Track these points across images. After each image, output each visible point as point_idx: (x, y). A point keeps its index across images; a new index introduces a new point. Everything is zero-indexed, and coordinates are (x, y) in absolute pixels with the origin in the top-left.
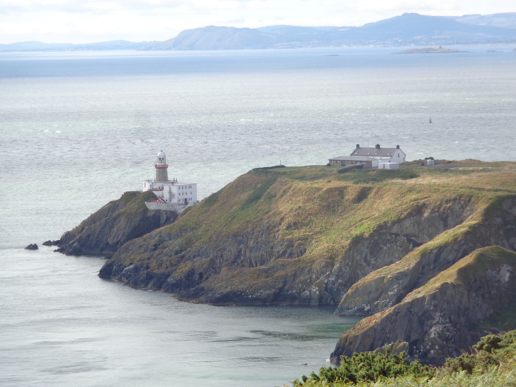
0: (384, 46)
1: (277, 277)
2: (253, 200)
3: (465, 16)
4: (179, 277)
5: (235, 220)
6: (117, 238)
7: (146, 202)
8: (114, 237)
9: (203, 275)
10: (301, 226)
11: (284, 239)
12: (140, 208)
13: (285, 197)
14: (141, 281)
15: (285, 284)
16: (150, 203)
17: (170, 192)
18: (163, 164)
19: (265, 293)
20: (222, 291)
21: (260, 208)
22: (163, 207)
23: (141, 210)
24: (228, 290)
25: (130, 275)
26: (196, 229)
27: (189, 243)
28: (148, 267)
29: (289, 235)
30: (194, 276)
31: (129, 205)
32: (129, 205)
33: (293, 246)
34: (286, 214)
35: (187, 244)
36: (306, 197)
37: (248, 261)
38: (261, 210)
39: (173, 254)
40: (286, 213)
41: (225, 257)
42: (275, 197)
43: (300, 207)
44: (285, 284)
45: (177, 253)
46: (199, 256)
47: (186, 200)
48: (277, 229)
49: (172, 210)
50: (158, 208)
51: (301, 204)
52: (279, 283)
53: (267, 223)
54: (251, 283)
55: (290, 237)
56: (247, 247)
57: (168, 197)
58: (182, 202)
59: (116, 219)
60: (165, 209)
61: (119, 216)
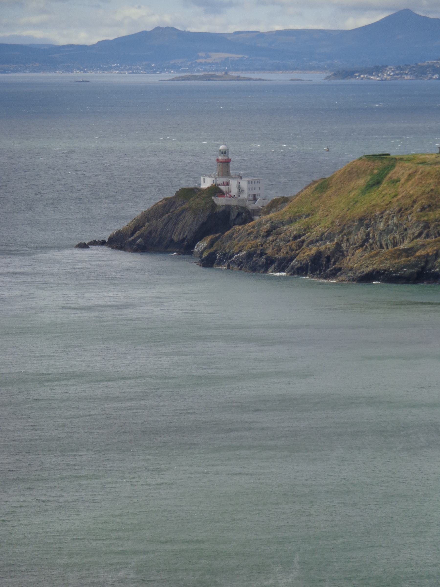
0: (133, 73)
1: (419, 257)
2: (374, 185)
3: (236, 33)
4: (305, 261)
5: (358, 204)
6: (184, 234)
7: (213, 198)
8: (180, 234)
9: (331, 258)
10: (436, 208)
11: (419, 221)
12: (208, 203)
13: (413, 180)
14: (260, 266)
15: (427, 262)
16: (218, 198)
17: (239, 188)
18: (226, 158)
19: (408, 271)
20: (362, 270)
21: (384, 192)
22: (233, 203)
23: (208, 205)
24: (370, 268)
25: (242, 262)
26: (312, 215)
27: (308, 228)
28: (262, 254)
29: (425, 216)
30: (321, 260)
31: (193, 201)
32: (193, 201)
33: (429, 228)
34: (418, 197)
35: (305, 230)
36: (436, 180)
37: (378, 244)
38: (386, 194)
39: (291, 239)
40: (417, 195)
41: (351, 241)
42: (399, 181)
43: (432, 190)
44: (427, 262)
45: (295, 238)
46: (321, 240)
47: (255, 195)
48: (409, 211)
49: (243, 206)
50: (228, 203)
51: (432, 187)
52: (421, 262)
53: (398, 206)
54: (393, 263)
55: (426, 218)
56: (375, 230)
57: (237, 192)
58: (251, 197)
59: (180, 215)
60: (235, 205)
61: (183, 211)
